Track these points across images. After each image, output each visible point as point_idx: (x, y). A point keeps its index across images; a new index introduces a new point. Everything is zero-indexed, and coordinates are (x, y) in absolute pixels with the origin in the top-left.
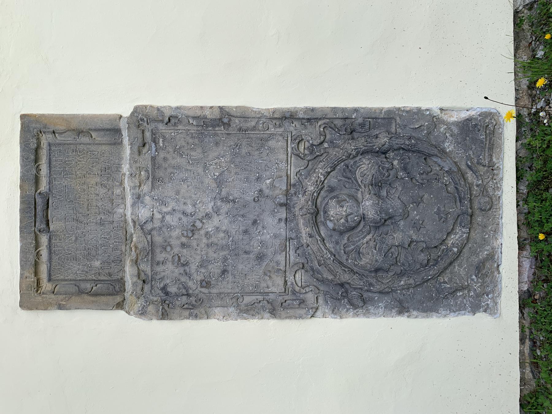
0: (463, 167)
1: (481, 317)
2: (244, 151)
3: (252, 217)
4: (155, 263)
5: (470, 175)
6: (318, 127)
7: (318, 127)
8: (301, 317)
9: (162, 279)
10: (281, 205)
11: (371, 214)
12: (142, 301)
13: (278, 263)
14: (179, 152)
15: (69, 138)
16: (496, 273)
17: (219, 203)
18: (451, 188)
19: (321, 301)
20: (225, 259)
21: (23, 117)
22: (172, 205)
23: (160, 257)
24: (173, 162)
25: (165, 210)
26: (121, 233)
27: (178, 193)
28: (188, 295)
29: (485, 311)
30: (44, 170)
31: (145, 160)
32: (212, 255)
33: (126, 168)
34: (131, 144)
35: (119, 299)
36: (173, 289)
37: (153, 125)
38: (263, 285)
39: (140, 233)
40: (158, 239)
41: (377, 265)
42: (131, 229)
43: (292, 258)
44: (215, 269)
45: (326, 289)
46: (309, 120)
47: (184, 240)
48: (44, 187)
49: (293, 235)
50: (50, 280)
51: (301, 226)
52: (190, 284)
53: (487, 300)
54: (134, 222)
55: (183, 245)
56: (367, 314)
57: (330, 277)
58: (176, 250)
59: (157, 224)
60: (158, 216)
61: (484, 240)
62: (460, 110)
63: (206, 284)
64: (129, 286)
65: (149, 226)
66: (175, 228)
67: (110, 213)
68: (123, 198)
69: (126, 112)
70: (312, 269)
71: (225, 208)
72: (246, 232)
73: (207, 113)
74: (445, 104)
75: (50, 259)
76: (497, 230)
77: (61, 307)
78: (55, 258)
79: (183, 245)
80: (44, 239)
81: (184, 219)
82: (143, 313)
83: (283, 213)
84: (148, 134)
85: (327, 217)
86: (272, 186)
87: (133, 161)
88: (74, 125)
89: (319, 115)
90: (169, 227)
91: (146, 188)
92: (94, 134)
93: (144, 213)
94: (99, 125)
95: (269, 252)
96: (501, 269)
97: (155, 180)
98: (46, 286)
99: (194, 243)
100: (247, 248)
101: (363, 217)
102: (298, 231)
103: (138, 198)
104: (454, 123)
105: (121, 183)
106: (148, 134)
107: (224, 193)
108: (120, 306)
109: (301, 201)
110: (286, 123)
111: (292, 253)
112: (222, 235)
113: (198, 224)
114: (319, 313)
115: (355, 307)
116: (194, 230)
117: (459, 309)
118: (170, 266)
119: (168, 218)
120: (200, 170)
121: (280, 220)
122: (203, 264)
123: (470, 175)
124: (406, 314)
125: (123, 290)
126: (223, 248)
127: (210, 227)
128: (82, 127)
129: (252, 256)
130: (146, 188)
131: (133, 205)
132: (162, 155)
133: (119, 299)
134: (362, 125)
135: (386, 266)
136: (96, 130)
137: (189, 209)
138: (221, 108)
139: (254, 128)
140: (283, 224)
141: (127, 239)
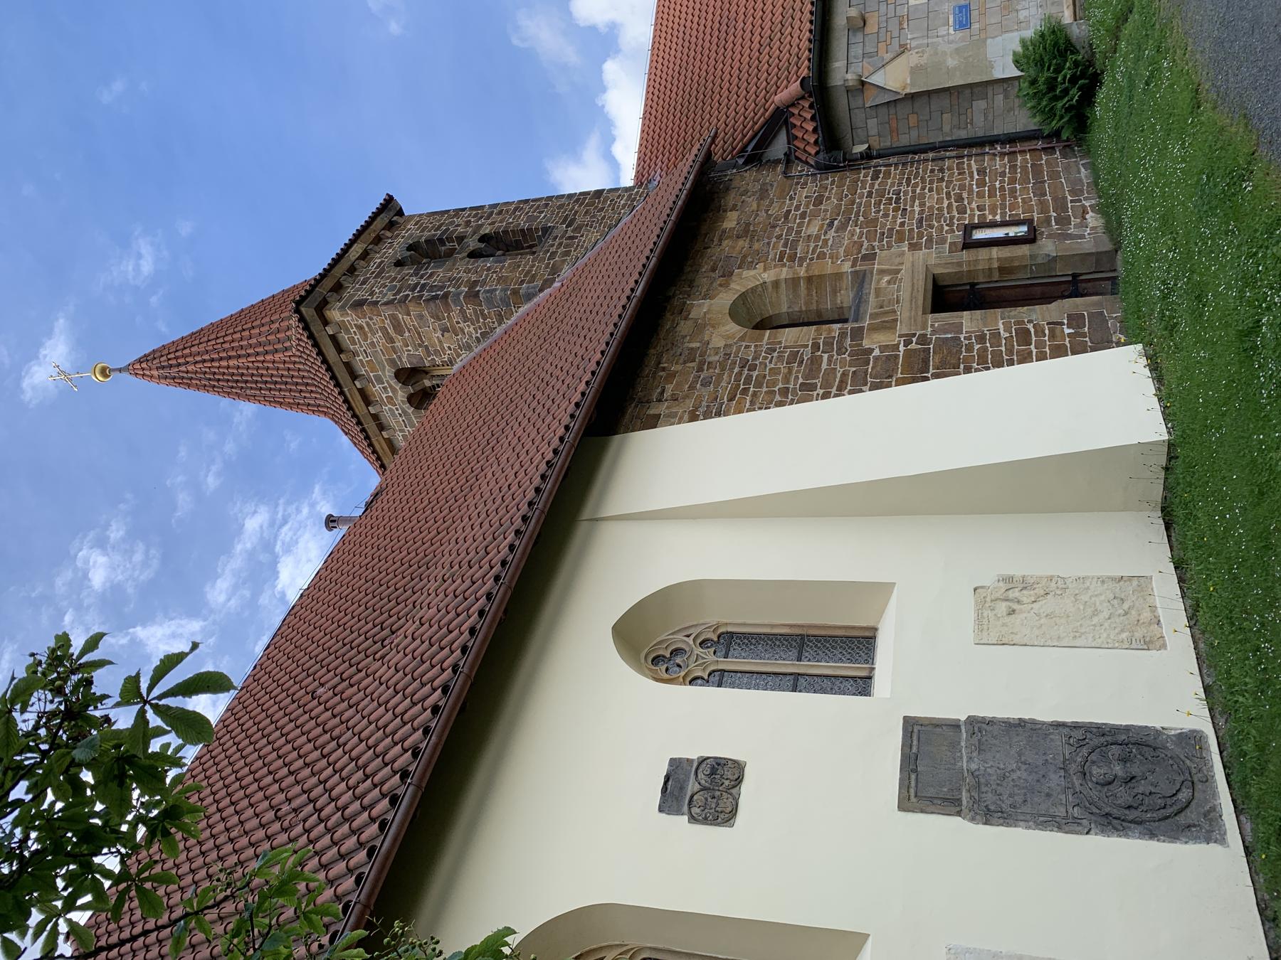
0: (1183, 758)
1: (1213, 847)
2: (1034, 739)
3: (1042, 773)
4: (980, 792)
5: (1188, 762)
6: (1082, 731)
7: (1082, 731)
8: (1077, 833)
9: (985, 801)
10: (1061, 768)
11: (1120, 773)
12: (972, 813)
13: (1061, 800)
14: (995, 737)
15: (929, 728)
16: (1219, 820)
17: (1020, 764)
18: (1175, 767)
19: (1093, 826)
20: (1025, 794)
21: (906, 719)
22: (991, 763)
23: (984, 789)
24: (991, 742)
25: (986, 765)
26: (960, 776)
27: (994, 757)
28: (1002, 812)
29: (1215, 842)
30: (915, 743)
31: (975, 740)
32: (1016, 791)
33: (963, 744)
34: (966, 732)
35: (958, 809)
36: (992, 808)
37: (979, 725)
38: (1051, 810)
39: (971, 777)
40: (982, 780)
41: (1129, 804)
42: (966, 774)
43: (1070, 799)
44: (1019, 799)
45: (1095, 819)
46: (1075, 727)
47: (999, 782)
48: (914, 749)
49: (1070, 786)
50: (916, 796)
51: (1075, 781)
52: (1003, 805)
53: (1215, 835)
54: (968, 770)
55: (998, 784)
56: (1127, 836)
57: (1098, 811)
58: (994, 787)
59: (982, 772)
60: (982, 768)
61: (1206, 799)
62: (1176, 729)
63: (1013, 806)
64: (964, 802)
65: (977, 773)
66: (993, 775)
67: (955, 764)
68: (961, 758)
69: (963, 718)
70: (1085, 807)
71: (1024, 767)
72: (1038, 781)
73: (1011, 721)
74: (1165, 725)
75: (916, 786)
76: (1215, 795)
77: (922, 811)
78: (920, 785)
79: (998, 784)
80: (913, 776)
81: (998, 771)
82: (973, 820)
83: (1062, 773)
84: (976, 729)
85: (1091, 775)
86: (1054, 758)
87: (967, 740)
88: (934, 722)
89: (1080, 725)
90: (989, 774)
91: (975, 754)
92: (944, 728)
93: (973, 766)
94: (948, 723)
95: (1054, 794)
96: (1223, 818)
97: (980, 751)
98: (913, 799)
99: (1005, 784)
100: (1040, 789)
101: (1116, 776)
102: (1073, 784)
103: (970, 759)
104: (1173, 735)
105: (960, 751)
106: (976, 729)
107: (1023, 759)
108: (959, 814)
109: (1073, 768)
110: (1061, 729)
111: (1070, 796)
112: (1022, 781)
113: (1007, 774)
114: (1092, 832)
115: (1117, 830)
116: (1004, 777)
117: (1196, 839)
118: (990, 795)
119: (988, 770)
120: (1008, 747)
121: (1060, 776)
122: (1011, 796)
123: (1188, 762)
124: (1040, 261)
125: (960, 805)
126: (1023, 788)
127: (1014, 776)
128: (937, 723)
129: (1043, 794)
130: (975, 754)
131: (968, 762)
132: (984, 739)
133: (958, 809)
134: (1110, 732)
135: (1135, 805)
136: (946, 725)
137: (1002, 766)
138: (1020, 719)
139: (1040, 729)
140: (1063, 779)
141: (964, 779)
